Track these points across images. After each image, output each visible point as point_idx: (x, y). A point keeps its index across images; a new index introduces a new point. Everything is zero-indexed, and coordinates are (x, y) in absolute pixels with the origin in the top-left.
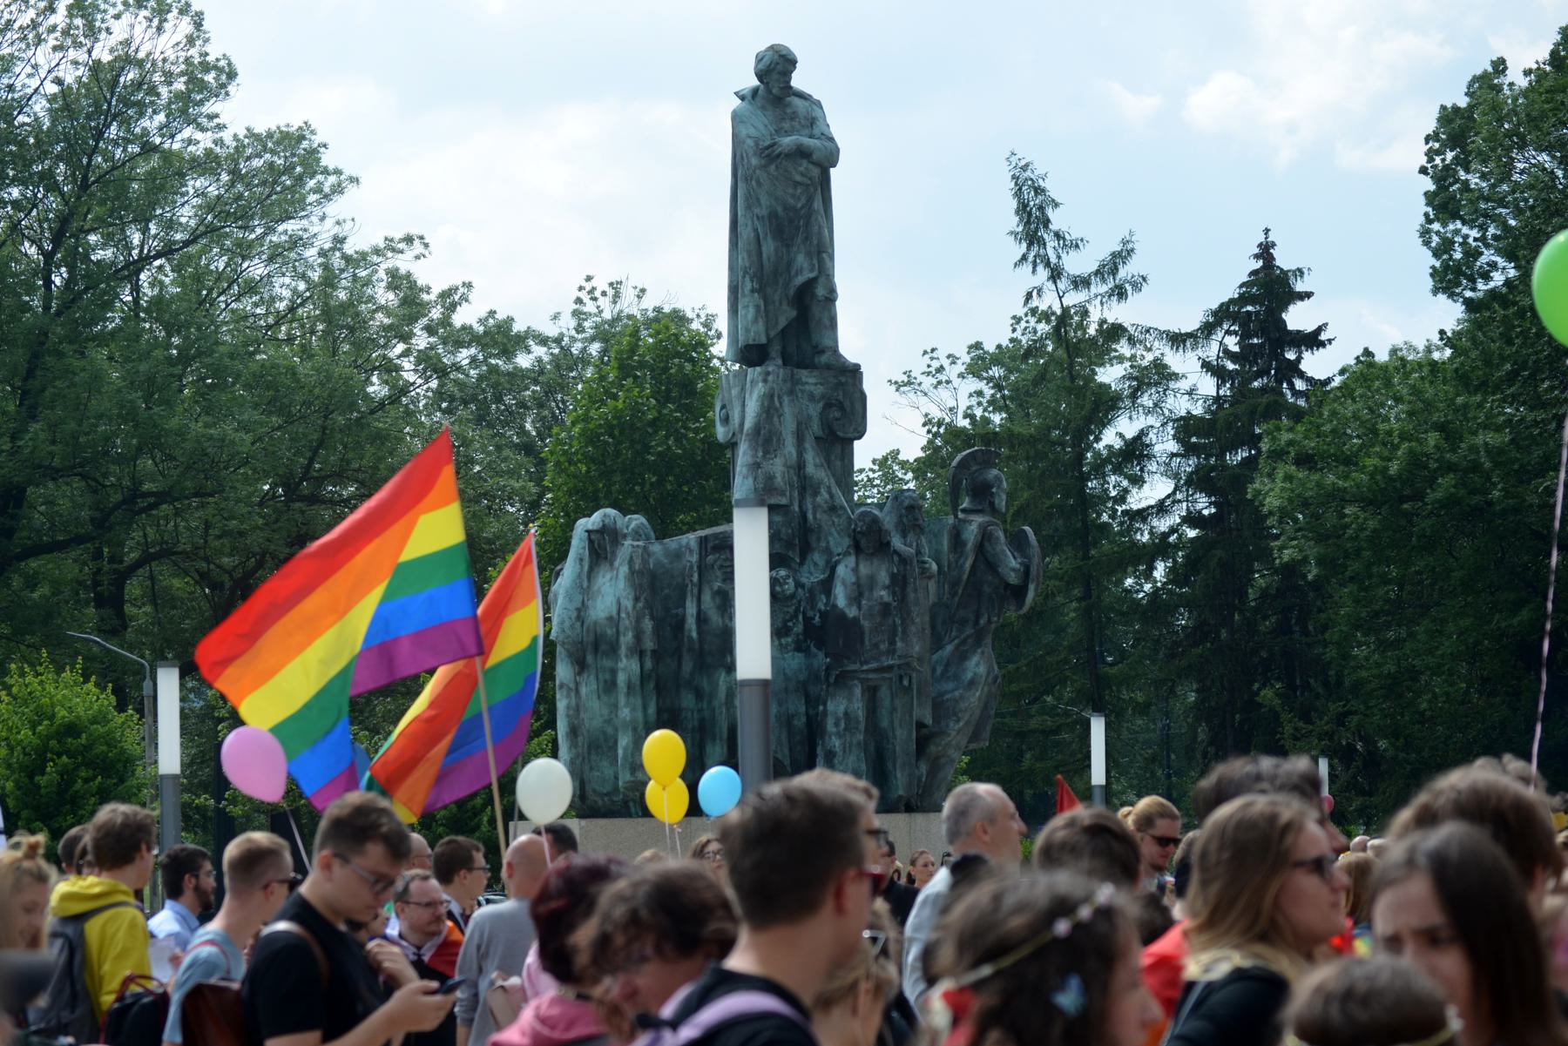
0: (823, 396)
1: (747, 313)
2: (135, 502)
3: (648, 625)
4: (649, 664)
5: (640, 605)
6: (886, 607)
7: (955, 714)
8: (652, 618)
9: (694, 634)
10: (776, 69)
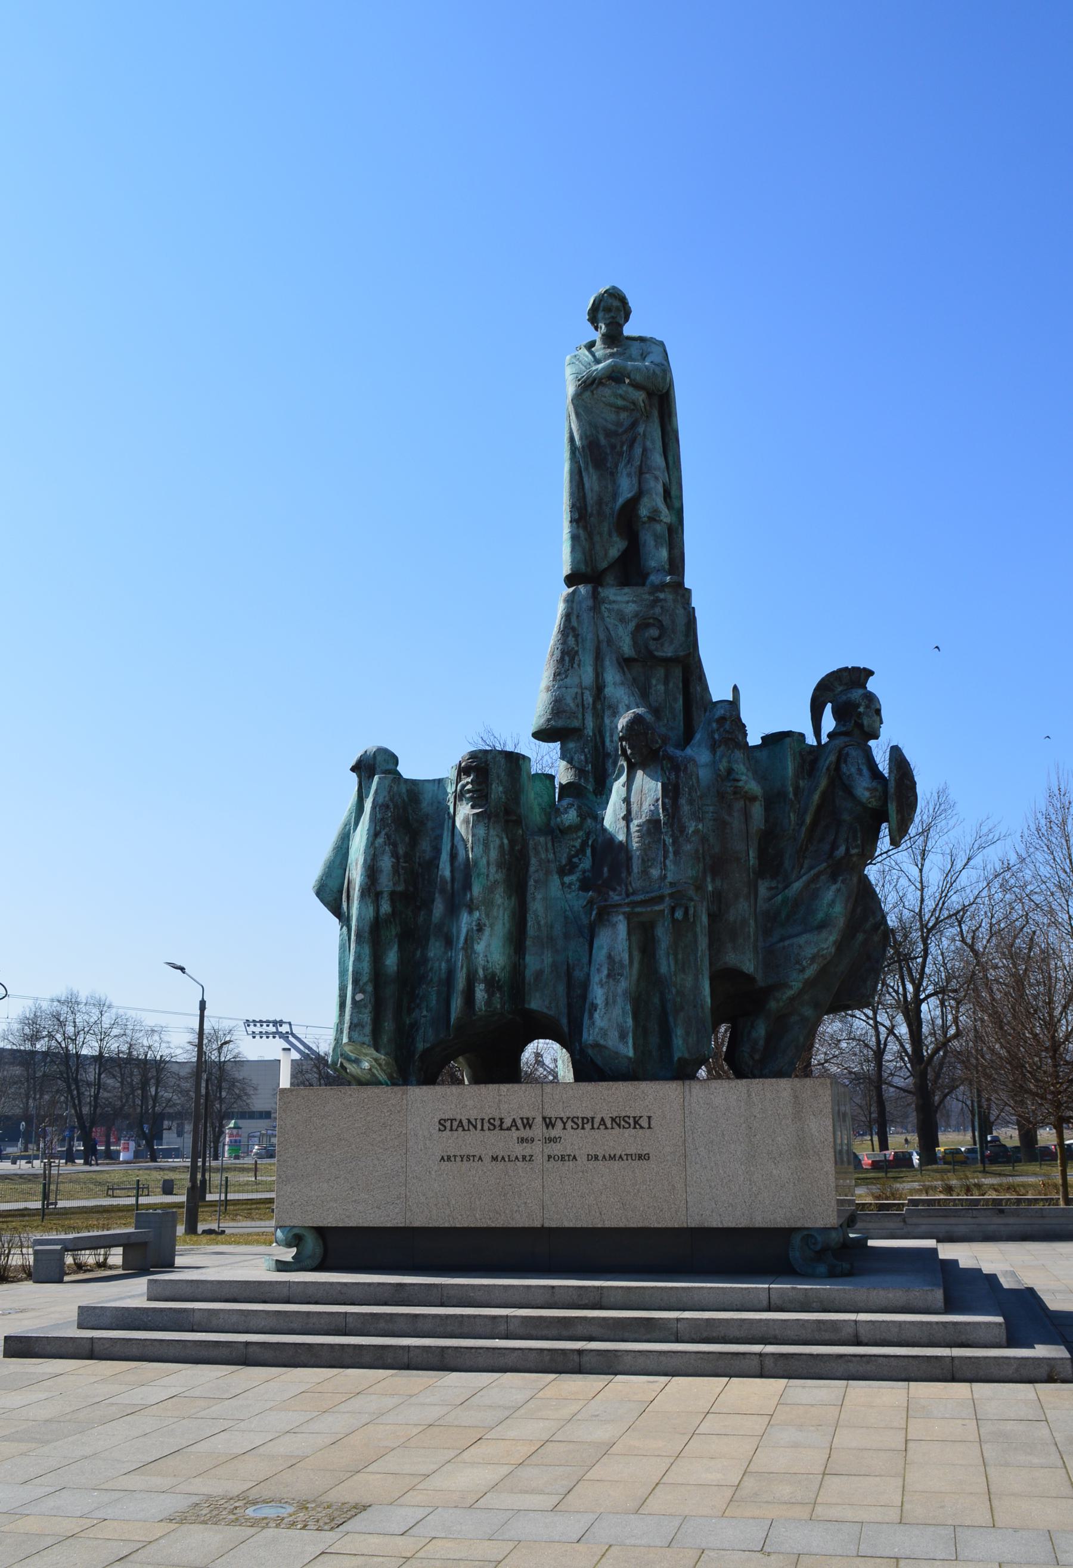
0: (636, 615)
2: (920, 914)
3: (386, 863)
4: (386, 907)
5: (380, 840)
7: (798, 962)
8: (395, 854)
9: (447, 873)
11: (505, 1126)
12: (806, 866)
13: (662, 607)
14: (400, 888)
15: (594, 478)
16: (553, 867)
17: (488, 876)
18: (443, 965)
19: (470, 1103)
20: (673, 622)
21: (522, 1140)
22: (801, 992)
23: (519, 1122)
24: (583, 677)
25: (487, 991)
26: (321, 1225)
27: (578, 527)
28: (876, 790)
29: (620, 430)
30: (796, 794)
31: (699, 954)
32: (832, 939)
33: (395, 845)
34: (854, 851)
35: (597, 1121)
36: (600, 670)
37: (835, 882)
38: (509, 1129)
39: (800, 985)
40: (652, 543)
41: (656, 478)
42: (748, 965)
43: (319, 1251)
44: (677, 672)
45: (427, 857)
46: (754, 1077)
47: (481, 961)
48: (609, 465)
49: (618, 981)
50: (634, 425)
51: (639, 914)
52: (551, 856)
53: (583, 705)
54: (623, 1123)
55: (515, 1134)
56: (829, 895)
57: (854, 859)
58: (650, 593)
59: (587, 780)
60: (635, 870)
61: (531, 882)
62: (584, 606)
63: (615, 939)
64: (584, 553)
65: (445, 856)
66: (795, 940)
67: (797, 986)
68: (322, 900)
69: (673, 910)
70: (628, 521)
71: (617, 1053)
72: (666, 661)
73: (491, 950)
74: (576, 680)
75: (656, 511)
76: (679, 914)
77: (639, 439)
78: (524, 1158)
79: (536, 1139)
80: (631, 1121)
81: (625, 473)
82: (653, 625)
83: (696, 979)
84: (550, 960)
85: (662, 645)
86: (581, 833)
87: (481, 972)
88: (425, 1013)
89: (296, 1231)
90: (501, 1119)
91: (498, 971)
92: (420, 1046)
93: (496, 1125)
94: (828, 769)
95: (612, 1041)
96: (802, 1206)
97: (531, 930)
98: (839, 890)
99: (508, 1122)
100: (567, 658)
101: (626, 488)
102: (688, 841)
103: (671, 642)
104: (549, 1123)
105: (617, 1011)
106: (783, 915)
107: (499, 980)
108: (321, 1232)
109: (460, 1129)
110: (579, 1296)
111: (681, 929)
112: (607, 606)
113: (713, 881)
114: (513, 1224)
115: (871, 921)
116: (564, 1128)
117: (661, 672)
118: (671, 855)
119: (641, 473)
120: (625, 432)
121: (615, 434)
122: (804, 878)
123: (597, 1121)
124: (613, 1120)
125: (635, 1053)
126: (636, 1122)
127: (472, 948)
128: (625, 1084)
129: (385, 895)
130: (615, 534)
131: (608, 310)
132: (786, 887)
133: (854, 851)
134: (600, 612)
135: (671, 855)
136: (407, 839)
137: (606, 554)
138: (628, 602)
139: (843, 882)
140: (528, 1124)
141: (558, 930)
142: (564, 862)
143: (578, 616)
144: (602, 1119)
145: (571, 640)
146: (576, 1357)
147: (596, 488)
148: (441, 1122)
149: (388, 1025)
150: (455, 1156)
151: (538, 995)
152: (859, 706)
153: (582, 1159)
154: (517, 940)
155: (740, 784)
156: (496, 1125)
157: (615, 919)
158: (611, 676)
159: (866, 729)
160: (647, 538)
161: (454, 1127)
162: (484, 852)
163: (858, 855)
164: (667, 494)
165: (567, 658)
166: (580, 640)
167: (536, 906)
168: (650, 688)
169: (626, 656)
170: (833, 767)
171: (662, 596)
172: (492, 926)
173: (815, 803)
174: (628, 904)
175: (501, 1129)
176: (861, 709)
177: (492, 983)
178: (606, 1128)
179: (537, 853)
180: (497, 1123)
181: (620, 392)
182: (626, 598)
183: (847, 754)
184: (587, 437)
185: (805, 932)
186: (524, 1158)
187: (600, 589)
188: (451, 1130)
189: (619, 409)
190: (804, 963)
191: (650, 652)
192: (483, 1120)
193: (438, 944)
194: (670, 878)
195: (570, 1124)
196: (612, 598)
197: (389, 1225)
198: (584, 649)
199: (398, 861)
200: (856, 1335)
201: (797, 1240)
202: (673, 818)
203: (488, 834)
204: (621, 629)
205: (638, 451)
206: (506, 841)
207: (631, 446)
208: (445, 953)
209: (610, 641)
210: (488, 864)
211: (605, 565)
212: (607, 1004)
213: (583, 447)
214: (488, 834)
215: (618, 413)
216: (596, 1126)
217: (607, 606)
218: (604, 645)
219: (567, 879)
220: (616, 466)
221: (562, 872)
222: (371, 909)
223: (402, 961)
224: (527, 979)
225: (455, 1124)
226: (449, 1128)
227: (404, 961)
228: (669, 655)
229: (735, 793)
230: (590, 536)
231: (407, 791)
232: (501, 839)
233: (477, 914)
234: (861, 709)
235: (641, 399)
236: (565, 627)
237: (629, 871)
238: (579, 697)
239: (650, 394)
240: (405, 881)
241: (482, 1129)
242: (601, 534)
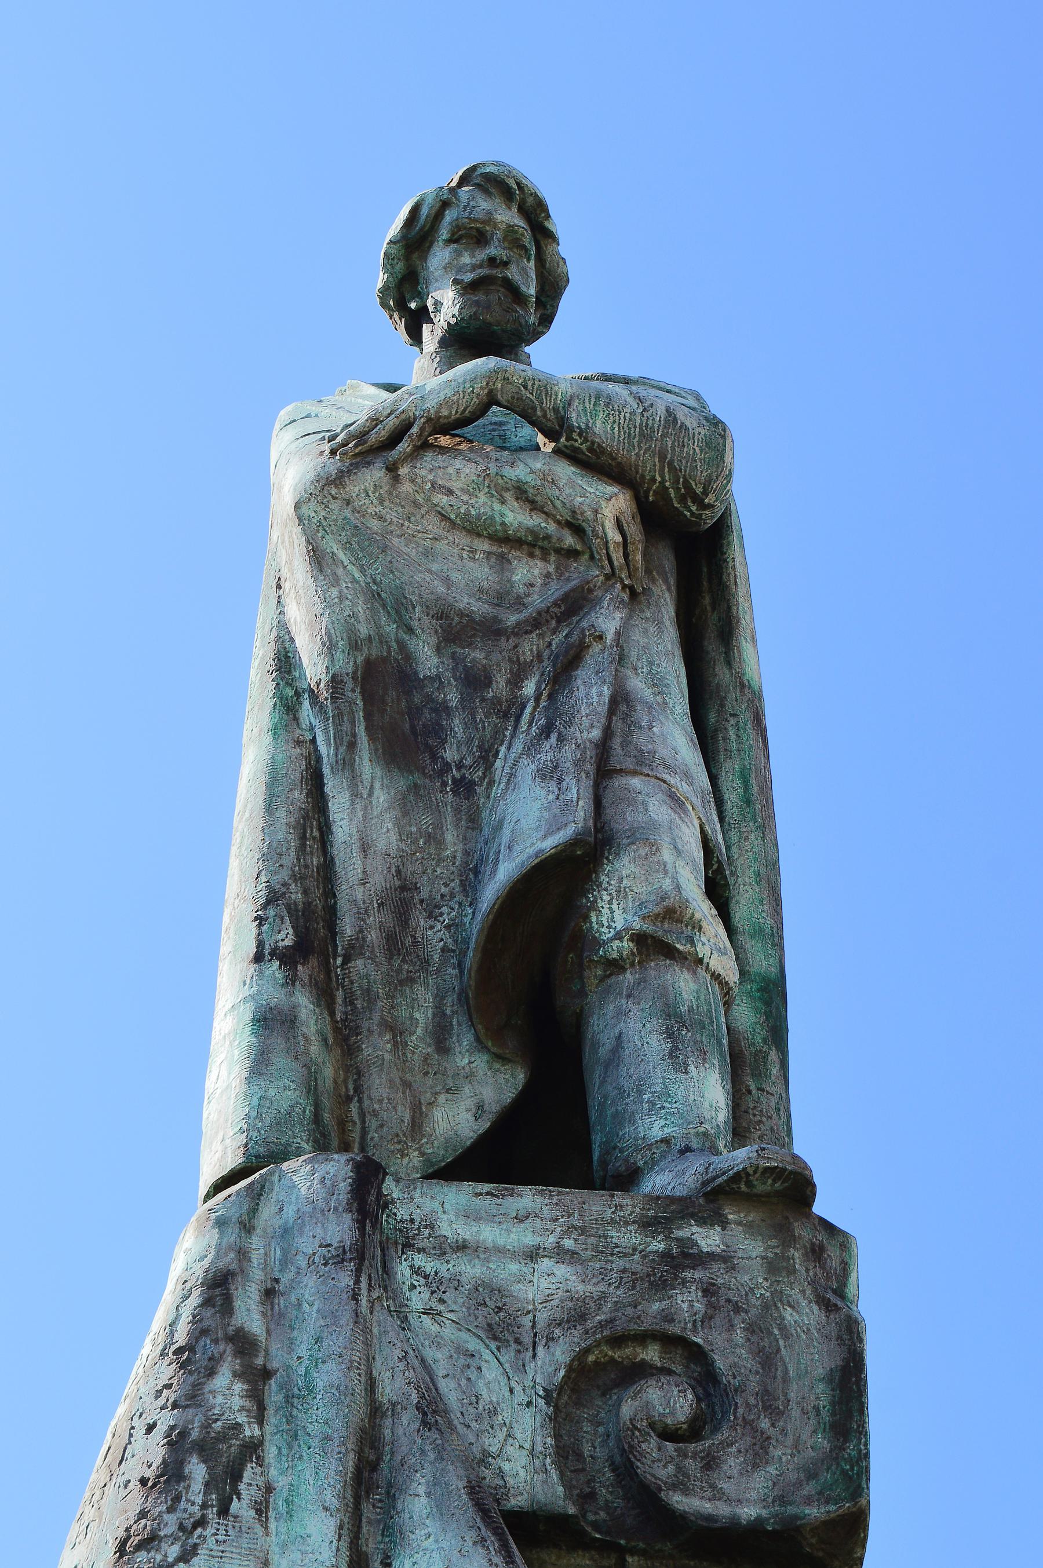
0: (576, 1315)
13: (709, 1291)
15: (381, 797)
20: (768, 1360)
27: (291, 980)
40: (656, 1045)
48: (450, 754)
50: (574, 604)
58: (647, 1225)
62: (307, 1244)
64: (311, 1086)
77: (596, 656)
81: (527, 770)
85: (710, 1463)
100: (197, 1471)
101: (530, 816)
103: (759, 1453)
112: (429, 1265)
119: (603, 769)
121: (491, 630)
130: (463, 1039)
131: (471, 235)
138: (533, 1255)
143: (269, 1294)
145: (227, 1393)
147: (386, 837)
160: (629, 1029)
165: (197, 1471)
166: (274, 1395)
169: (515, 1502)
171: (708, 1239)
182: (524, 1236)
184: (355, 645)
189: (508, 542)
191: (645, 1499)
196: (451, 1228)
204: (491, 1372)
205: (590, 693)
209: (431, 1411)
213: (335, 682)
215: (502, 558)
217: (429, 1265)
218: (403, 1429)
220: (487, 756)
228: (749, 1512)
230: (345, 1038)
236: (200, 1331)
242: (396, 1031)
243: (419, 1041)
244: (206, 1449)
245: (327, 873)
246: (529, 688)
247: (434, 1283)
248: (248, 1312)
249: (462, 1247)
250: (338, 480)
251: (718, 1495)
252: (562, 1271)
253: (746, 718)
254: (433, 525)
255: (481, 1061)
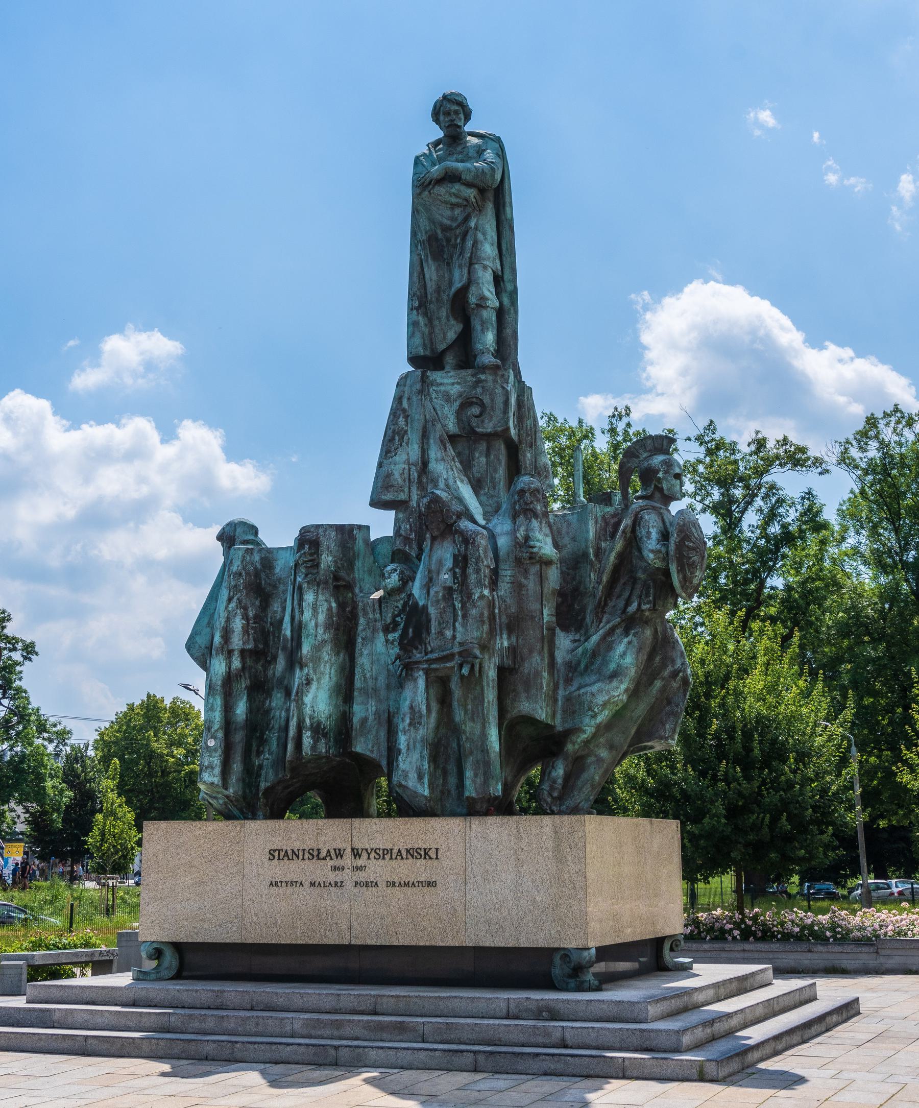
0: (460, 395)
1: (418, 340)
3: (238, 624)
4: (236, 663)
5: (233, 605)
6: (449, 591)
7: (590, 709)
8: (245, 617)
9: (288, 633)
10: (451, 112)
11: (321, 856)
12: (604, 620)
14: (250, 646)
15: (433, 268)
16: (379, 625)
17: (316, 636)
18: (283, 714)
19: (294, 836)
20: (493, 400)
21: (335, 868)
22: (595, 736)
23: (333, 853)
24: (411, 453)
25: (312, 737)
26: (175, 940)
28: (659, 551)
29: (455, 225)
30: (597, 555)
31: (486, 705)
32: (623, 687)
33: (245, 608)
34: (645, 607)
35: (395, 851)
36: (425, 447)
37: (627, 635)
38: (324, 859)
39: (593, 730)
41: (485, 267)
42: (541, 713)
43: (175, 964)
44: (501, 449)
45: (278, 617)
46: (173, 819)
47: (308, 711)
49: (418, 729)
50: (467, 219)
51: (436, 670)
52: (378, 616)
53: (409, 479)
54: (415, 854)
55: (330, 863)
56: (621, 648)
57: (647, 614)
59: (410, 547)
60: (433, 631)
61: (359, 640)
63: (417, 693)
65: (287, 618)
66: (588, 689)
67: (589, 731)
68: (192, 656)
69: (461, 666)
70: (462, 307)
71: (415, 792)
72: (489, 437)
73: (318, 701)
74: (404, 457)
75: (483, 298)
76: (465, 671)
77: (470, 233)
78: (336, 884)
79: (346, 868)
80: (422, 852)
82: (476, 403)
83: (484, 727)
84: (374, 708)
85: (483, 422)
86: (403, 595)
87: (308, 721)
88: (267, 756)
89: (155, 945)
90: (318, 850)
91: (323, 720)
92: (263, 785)
93: (315, 855)
94: (624, 532)
95: (411, 782)
96: (559, 929)
97: (358, 684)
98: (630, 643)
99: (323, 853)
101: (459, 279)
102: (474, 606)
104: (356, 854)
105: (415, 757)
106: (582, 666)
107: (325, 728)
108: (178, 947)
109: (286, 858)
110: (359, 1002)
111: (473, 680)
113: (509, 638)
114: (326, 942)
115: (670, 668)
116: (369, 858)
117: (483, 446)
118: (460, 618)
120: (459, 226)
122: (601, 632)
123: (395, 851)
124: (408, 851)
125: (430, 793)
126: (426, 854)
127: (302, 700)
128: (419, 819)
129: (236, 653)
132: (586, 640)
133: (645, 607)
134: (429, 394)
135: (460, 618)
136: (257, 603)
137: (444, 338)
138: (453, 384)
139: (634, 635)
140: (339, 854)
141: (382, 682)
142: (389, 621)
143: (409, 399)
144: (399, 851)
145: (401, 421)
146: (333, 1052)
147: (435, 277)
148: (271, 852)
149: (237, 767)
150: (281, 882)
151: (362, 739)
152: (658, 471)
153: (382, 886)
154: (345, 691)
155: (535, 550)
156: (315, 855)
157: (416, 675)
158: (434, 453)
159: (666, 492)
161: (281, 857)
162: (313, 615)
163: (649, 610)
164: (498, 280)
166: (409, 421)
167: (364, 661)
168: (473, 460)
170: (629, 530)
171: (483, 377)
172: (319, 680)
173: (611, 563)
174: (427, 661)
175: (318, 859)
176: (660, 475)
177: (318, 730)
178: (402, 858)
179: (365, 613)
180: (315, 853)
181: (453, 190)
183: (641, 518)
185: (598, 681)
186: (336, 884)
187: (429, 373)
188: (279, 859)
189: (453, 206)
190: (596, 710)
192: (304, 850)
193: (279, 695)
194: (459, 638)
195: (373, 854)
197: (228, 941)
198: (412, 428)
199: (248, 622)
200: (563, 1040)
201: (557, 959)
202: (462, 585)
203: (317, 600)
205: (469, 243)
206: (334, 605)
207: (464, 239)
208: (285, 703)
210: (316, 626)
211: (443, 346)
212: (408, 749)
214: (317, 600)
216: (394, 857)
219: (391, 637)
220: (451, 257)
221: (386, 630)
222: (224, 665)
223: (250, 711)
224: (354, 727)
225: (282, 854)
226: (277, 857)
227: (251, 710)
228: (489, 430)
229: (530, 558)
230: (430, 321)
231: (262, 559)
232: (330, 603)
233: (306, 670)
234: (660, 475)
235: (472, 196)
237: (429, 633)
238: (406, 472)
239: (482, 191)
240: (255, 640)
241: (303, 859)
242: (439, 319)
243: (444, 320)
244: (398, 433)
245: (425, 285)
246: (458, 241)
247: (436, 392)
248: (405, 404)
249: (441, 384)
250: (420, 194)
251: (484, 428)
252: (458, 387)
253: (507, 228)
254: (439, 203)
255: (455, 322)
